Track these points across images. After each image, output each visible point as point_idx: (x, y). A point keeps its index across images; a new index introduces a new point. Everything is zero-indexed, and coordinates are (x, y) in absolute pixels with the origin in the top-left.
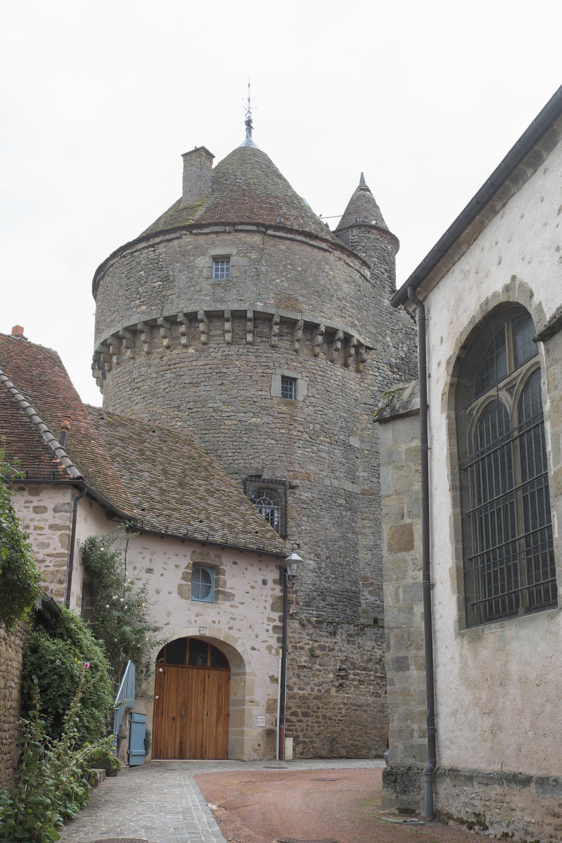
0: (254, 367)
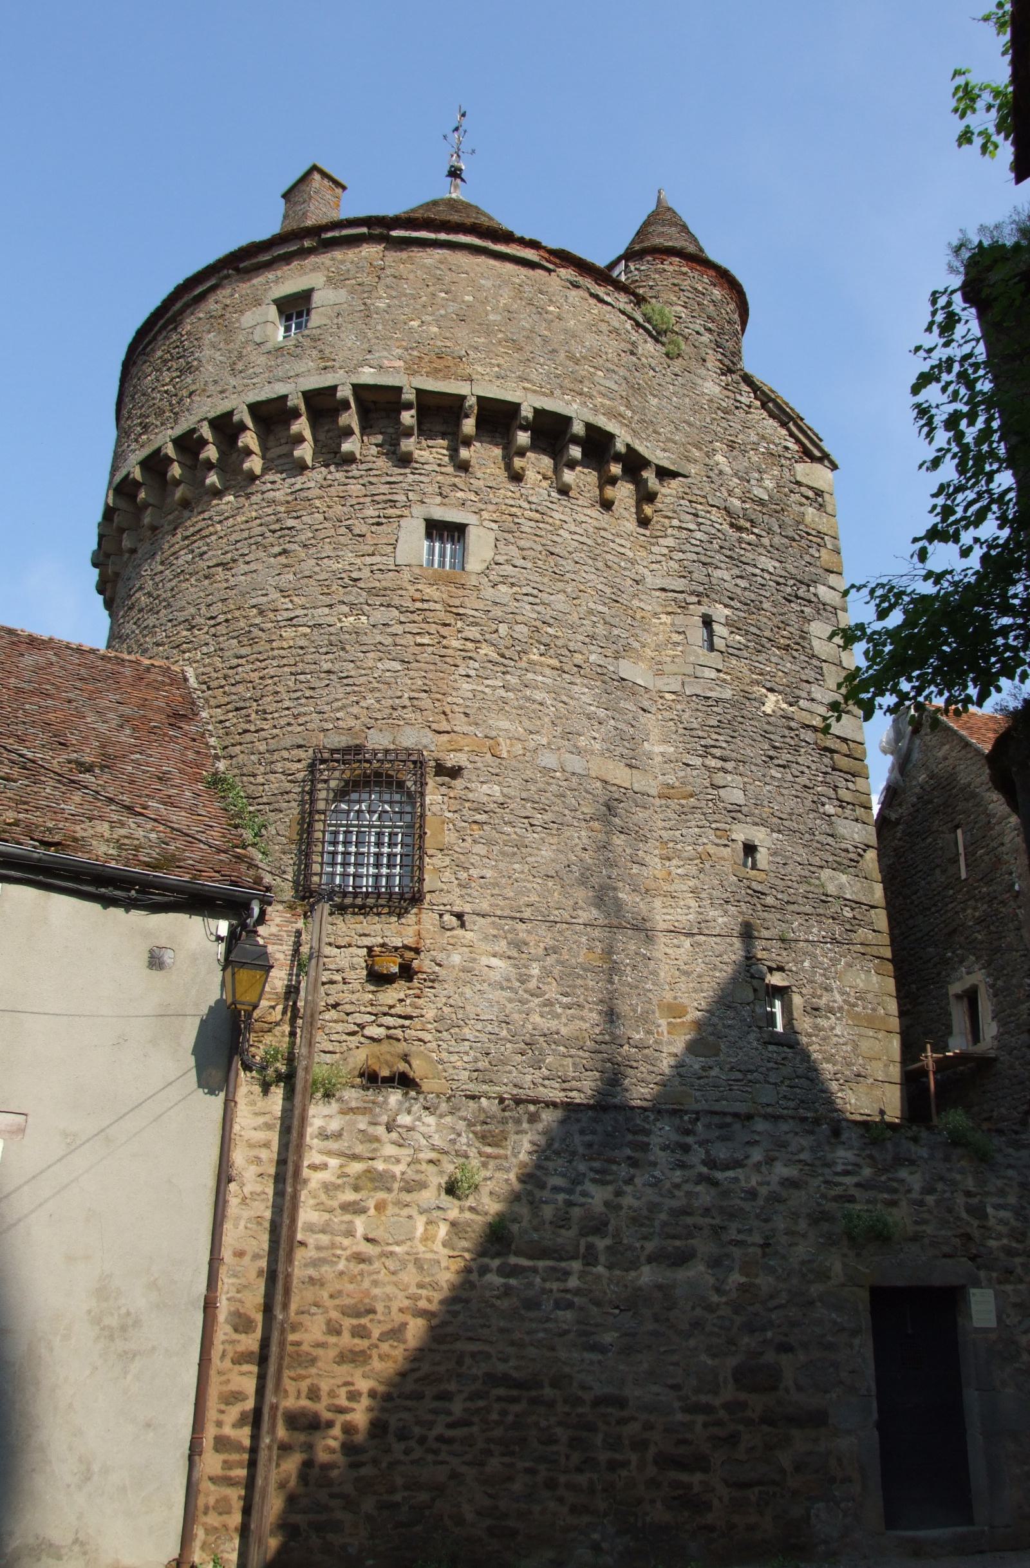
0: (356, 507)
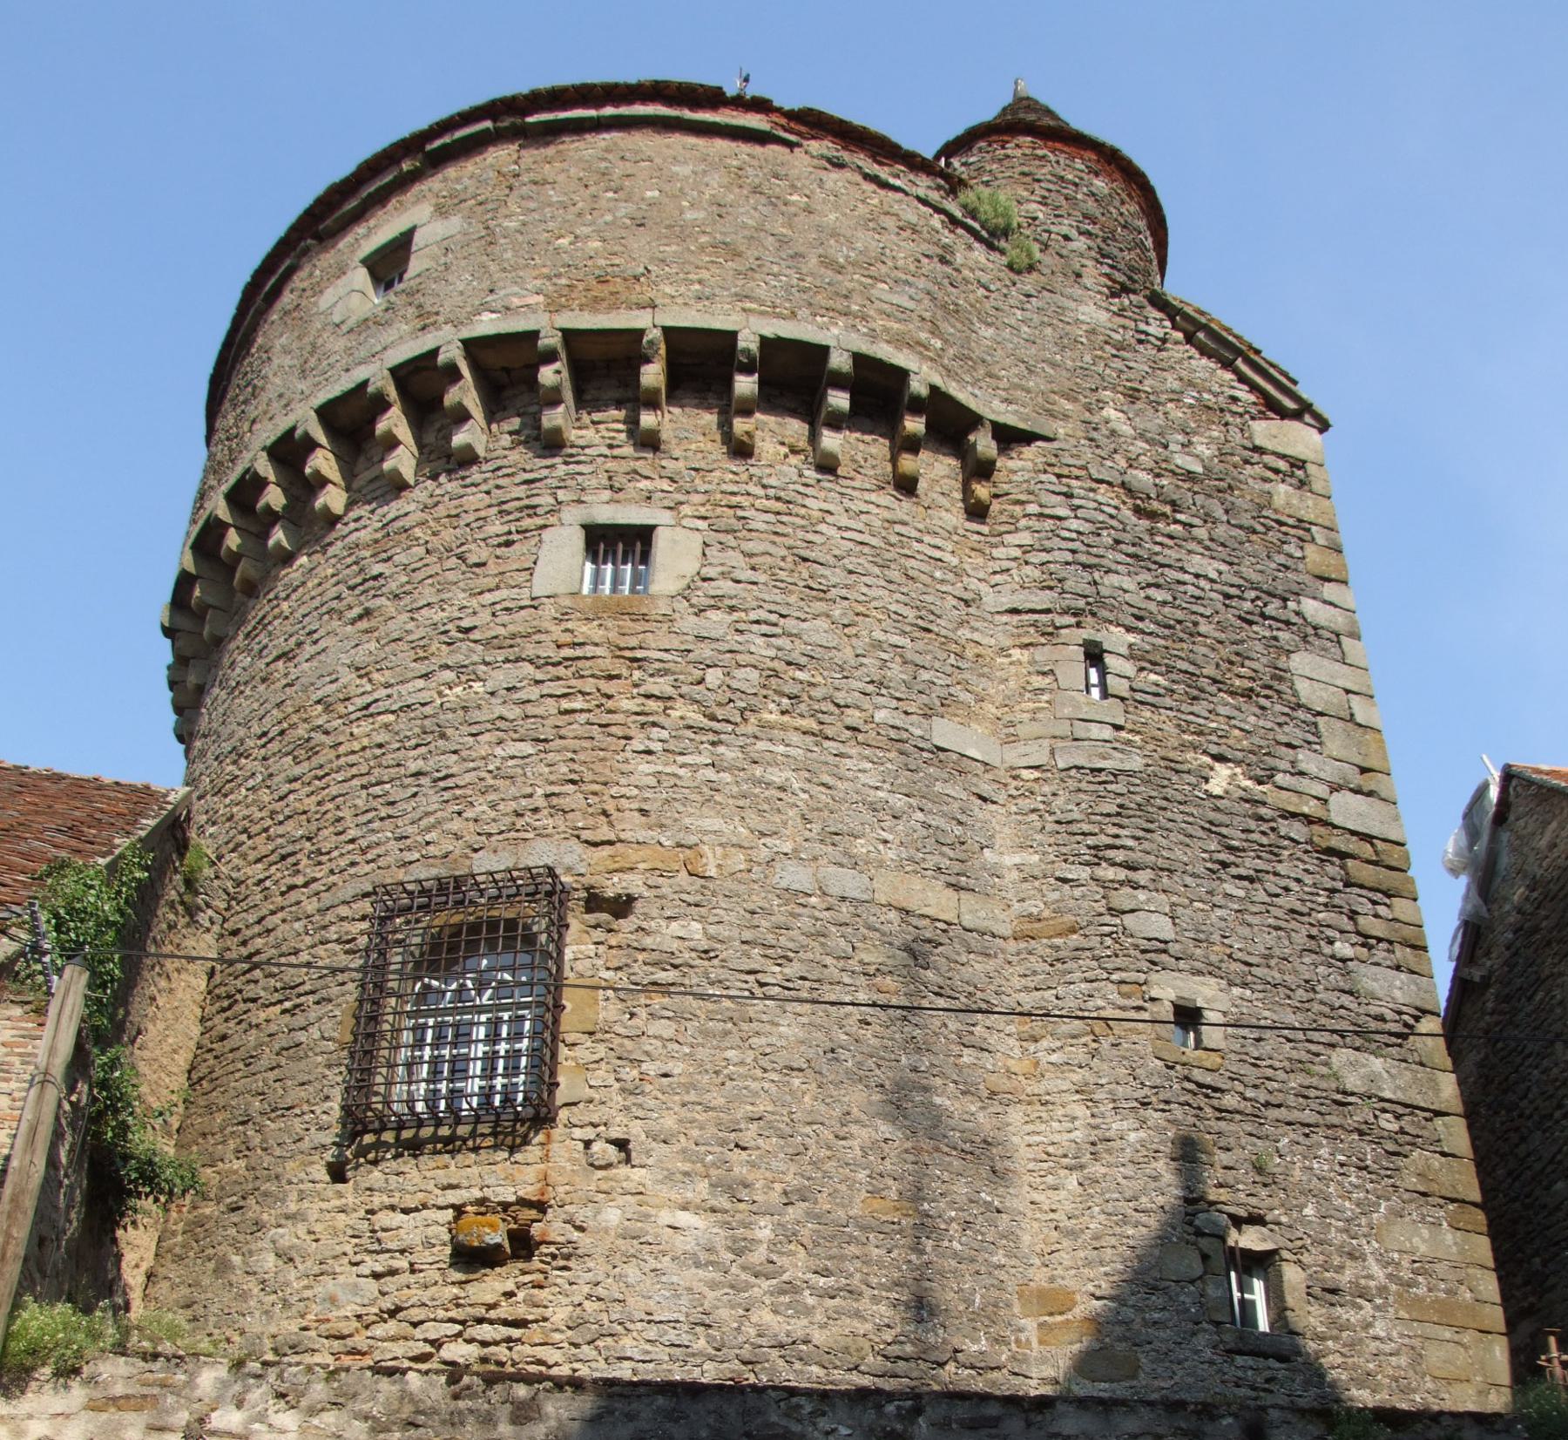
0: (474, 525)
